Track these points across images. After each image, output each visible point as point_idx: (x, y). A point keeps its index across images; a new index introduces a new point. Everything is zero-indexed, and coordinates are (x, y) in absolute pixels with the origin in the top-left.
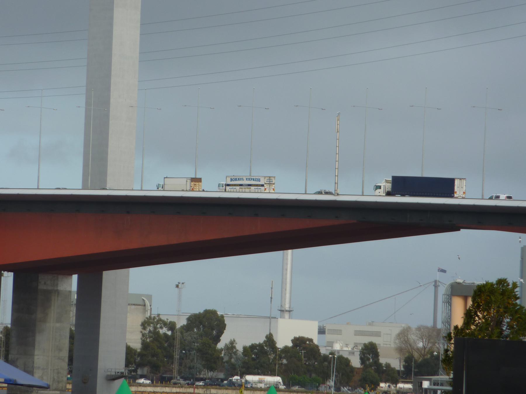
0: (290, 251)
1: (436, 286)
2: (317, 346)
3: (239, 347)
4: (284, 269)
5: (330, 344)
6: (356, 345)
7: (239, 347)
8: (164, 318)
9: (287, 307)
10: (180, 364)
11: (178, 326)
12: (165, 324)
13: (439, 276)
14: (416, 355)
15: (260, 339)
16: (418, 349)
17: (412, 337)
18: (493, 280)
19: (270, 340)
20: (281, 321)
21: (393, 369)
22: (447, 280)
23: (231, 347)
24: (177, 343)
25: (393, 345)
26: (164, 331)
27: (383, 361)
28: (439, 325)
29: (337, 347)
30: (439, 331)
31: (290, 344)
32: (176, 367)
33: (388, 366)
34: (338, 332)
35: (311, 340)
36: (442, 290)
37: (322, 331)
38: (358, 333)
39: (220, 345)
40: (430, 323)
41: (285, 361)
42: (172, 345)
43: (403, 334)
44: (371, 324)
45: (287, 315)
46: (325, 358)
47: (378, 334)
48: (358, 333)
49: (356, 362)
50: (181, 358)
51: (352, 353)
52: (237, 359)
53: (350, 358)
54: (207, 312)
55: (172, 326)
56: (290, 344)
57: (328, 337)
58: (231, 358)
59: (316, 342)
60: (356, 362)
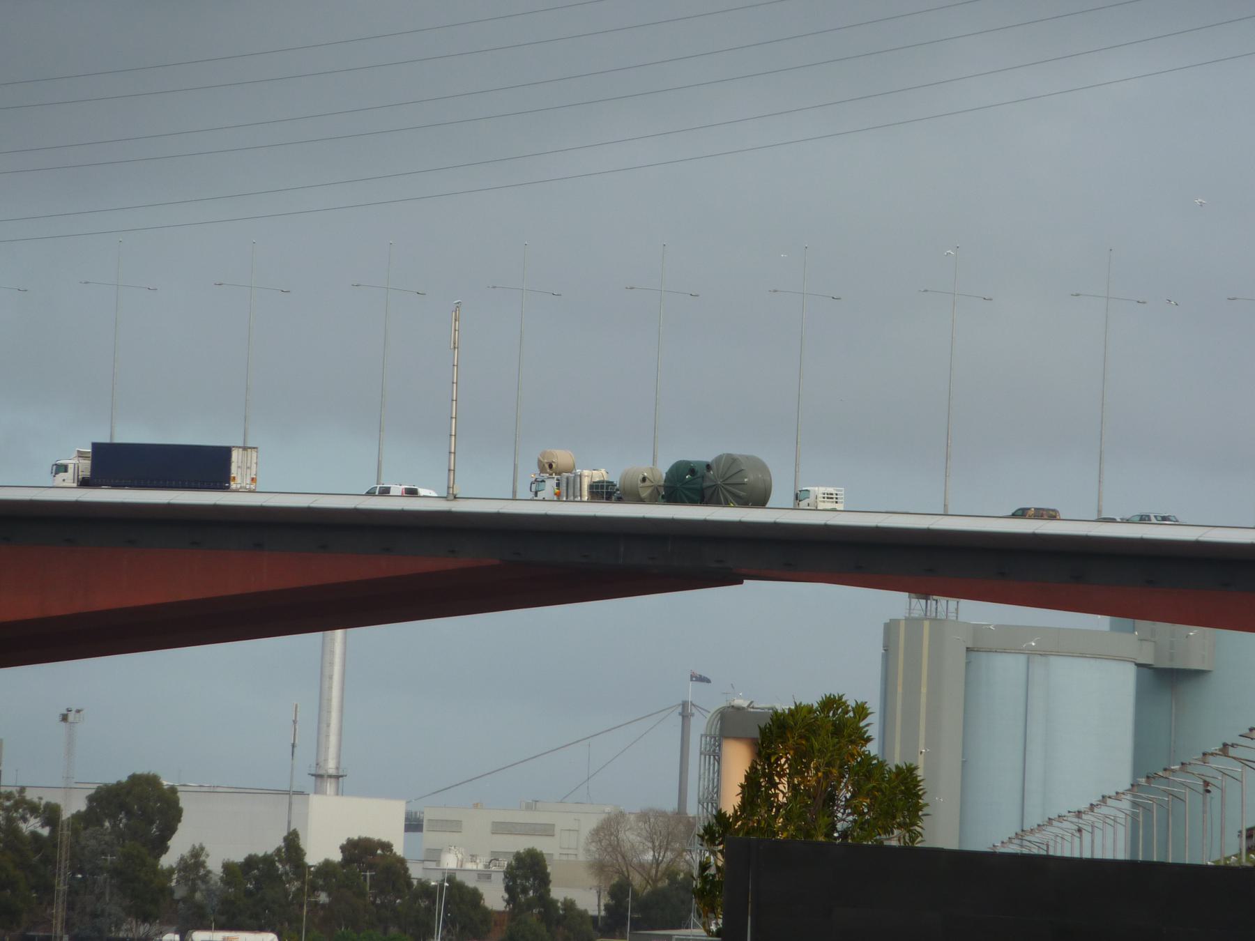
0: (339, 633)
1: (685, 716)
2: (402, 861)
3: (214, 865)
4: (323, 676)
5: (434, 855)
6: (495, 858)
7: (214, 865)
8: (31, 795)
9: (331, 766)
10: (71, 907)
11: (66, 814)
12: (33, 809)
13: (692, 692)
14: (637, 880)
15: (268, 843)
16: (642, 865)
17: (631, 837)
18: (812, 698)
19: (292, 846)
20: (315, 800)
21: (583, 915)
22: (711, 701)
23: (194, 863)
24: (63, 855)
25: (582, 857)
26: (32, 825)
27: (558, 893)
28: (693, 809)
29: (450, 862)
30: (690, 825)
31: (337, 857)
32: (59, 911)
33: (569, 905)
34: (453, 826)
35: (387, 847)
36: (700, 725)
37: (413, 825)
38: (500, 828)
39: (168, 860)
40: (671, 805)
41: (323, 898)
42: (49, 861)
43: (608, 830)
44: (531, 806)
45: (330, 786)
46: (426, 891)
47: (547, 830)
48: (500, 828)
49: (495, 898)
50: (72, 892)
51: (485, 876)
52: (209, 893)
53: (483, 888)
54: (135, 780)
55: (51, 814)
56: (337, 857)
57: (429, 838)
58: (193, 889)
59: (399, 850)
60: (495, 898)
